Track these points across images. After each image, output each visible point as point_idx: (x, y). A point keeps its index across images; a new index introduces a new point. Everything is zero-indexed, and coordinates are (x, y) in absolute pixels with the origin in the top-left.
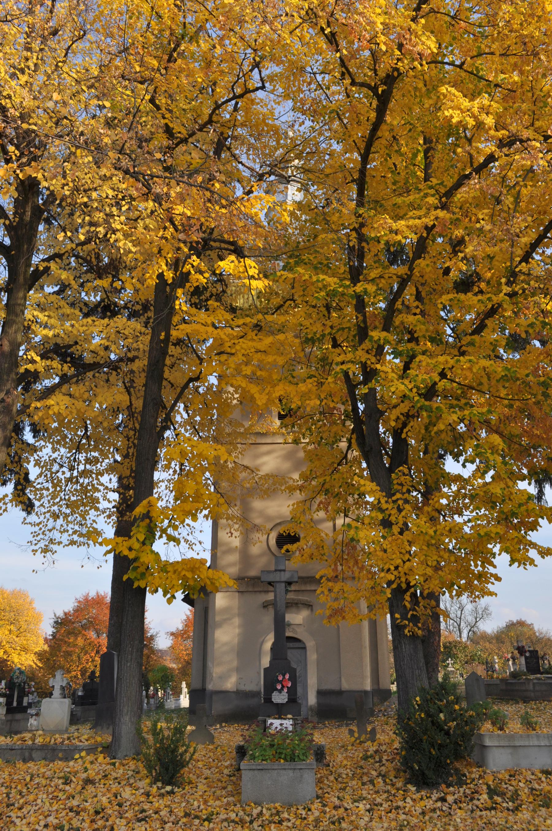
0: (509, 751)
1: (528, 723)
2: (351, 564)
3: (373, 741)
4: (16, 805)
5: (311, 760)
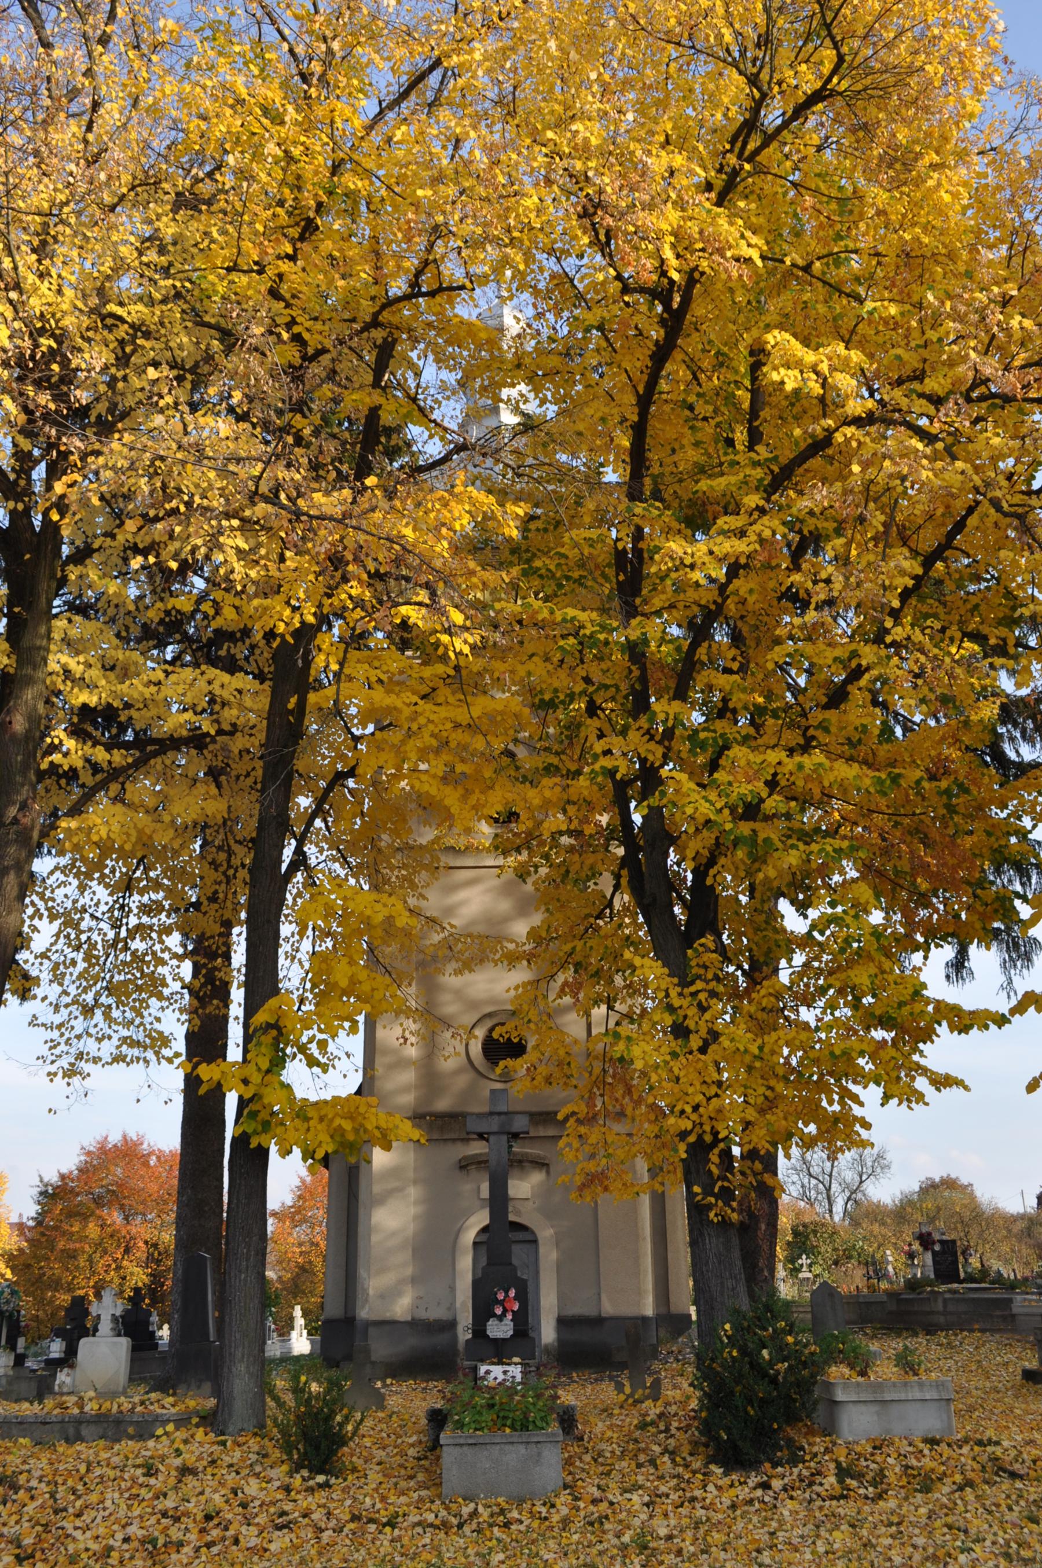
0: (874, 1408)
1: (907, 1364)
2: (619, 1094)
3: (656, 1399)
4: (71, 1510)
5: (554, 1428)
